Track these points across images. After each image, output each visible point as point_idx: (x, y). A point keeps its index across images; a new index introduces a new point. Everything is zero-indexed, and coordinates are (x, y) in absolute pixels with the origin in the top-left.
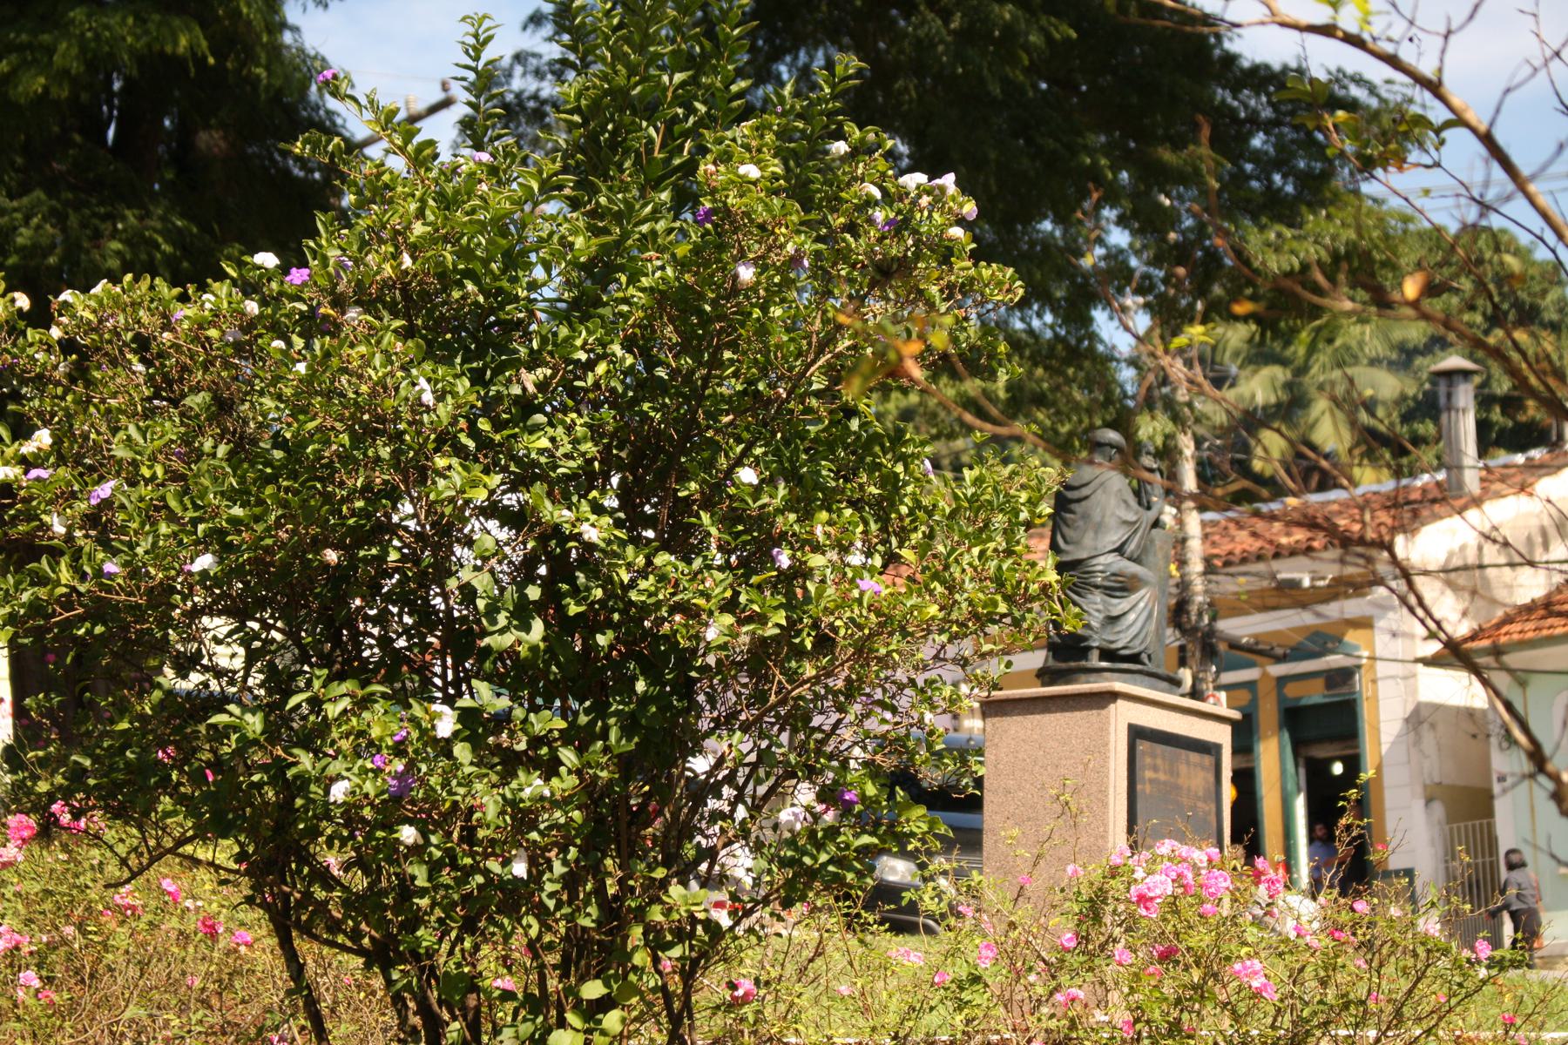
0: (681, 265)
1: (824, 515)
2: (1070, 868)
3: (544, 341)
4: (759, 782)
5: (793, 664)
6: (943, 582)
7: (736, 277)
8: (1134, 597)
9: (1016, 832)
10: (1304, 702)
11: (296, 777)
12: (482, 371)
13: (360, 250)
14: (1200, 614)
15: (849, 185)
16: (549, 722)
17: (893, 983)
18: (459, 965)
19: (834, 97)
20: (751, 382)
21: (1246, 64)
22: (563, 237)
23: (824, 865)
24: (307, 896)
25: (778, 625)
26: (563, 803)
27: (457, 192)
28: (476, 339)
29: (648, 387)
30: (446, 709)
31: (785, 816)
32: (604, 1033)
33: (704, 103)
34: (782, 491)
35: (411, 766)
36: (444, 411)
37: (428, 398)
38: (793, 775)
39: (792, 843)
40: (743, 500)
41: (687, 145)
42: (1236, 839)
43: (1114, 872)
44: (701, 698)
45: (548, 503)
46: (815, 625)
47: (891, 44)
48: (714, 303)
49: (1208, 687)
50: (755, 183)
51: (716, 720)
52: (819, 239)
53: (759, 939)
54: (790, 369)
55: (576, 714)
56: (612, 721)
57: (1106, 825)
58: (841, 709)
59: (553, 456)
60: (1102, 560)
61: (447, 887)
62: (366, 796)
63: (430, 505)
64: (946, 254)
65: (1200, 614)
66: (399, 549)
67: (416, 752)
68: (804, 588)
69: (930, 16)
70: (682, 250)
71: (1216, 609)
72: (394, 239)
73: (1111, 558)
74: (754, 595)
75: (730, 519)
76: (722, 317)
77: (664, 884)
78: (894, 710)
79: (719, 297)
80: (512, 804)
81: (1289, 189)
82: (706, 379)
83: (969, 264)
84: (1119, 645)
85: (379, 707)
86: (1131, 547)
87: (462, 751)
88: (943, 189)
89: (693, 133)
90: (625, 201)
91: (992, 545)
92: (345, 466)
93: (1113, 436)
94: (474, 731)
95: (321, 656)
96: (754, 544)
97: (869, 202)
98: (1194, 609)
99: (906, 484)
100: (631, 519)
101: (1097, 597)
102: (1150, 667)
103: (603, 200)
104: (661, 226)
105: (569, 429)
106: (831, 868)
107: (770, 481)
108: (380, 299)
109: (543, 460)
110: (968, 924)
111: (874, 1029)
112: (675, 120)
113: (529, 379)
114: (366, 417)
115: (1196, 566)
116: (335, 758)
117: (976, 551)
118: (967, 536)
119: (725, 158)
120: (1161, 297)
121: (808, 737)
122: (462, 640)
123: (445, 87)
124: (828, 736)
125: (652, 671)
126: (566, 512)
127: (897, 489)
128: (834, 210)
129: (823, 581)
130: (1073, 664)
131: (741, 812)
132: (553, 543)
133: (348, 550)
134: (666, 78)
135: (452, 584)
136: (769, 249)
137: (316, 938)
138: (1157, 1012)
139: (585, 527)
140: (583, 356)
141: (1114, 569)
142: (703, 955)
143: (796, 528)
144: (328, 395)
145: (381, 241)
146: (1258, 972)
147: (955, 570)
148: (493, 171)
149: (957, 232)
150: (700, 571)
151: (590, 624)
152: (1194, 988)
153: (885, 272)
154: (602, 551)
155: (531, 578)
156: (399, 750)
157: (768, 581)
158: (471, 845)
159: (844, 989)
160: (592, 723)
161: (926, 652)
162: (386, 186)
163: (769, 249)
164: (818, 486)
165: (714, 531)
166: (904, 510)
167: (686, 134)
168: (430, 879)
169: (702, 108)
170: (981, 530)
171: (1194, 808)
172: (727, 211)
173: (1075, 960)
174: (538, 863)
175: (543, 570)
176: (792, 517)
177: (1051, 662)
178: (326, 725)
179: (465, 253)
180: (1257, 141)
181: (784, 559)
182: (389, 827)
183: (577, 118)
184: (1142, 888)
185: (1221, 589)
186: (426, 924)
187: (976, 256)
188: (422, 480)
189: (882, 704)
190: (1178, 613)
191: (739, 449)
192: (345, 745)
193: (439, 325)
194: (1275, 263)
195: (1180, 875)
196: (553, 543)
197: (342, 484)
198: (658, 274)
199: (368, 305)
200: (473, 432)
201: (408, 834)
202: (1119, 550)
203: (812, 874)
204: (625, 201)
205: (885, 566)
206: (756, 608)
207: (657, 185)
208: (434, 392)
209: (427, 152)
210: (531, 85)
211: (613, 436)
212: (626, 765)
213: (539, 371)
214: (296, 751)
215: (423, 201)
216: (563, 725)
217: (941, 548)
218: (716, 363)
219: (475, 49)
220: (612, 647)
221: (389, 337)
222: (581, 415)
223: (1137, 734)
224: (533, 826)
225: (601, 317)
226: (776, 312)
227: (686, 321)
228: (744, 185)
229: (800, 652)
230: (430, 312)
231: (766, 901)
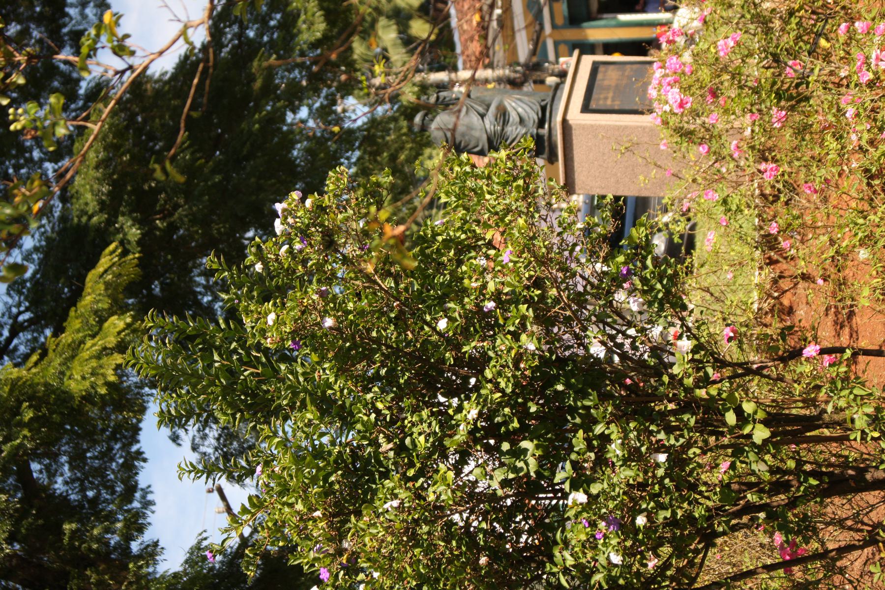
0: (323, 358)
1: (466, 281)
2: (662, 147)
3: (364, 438)
4: (615, 322)
5: (549, 301)
6: (506, 215)
7: (331, 328)
8: (509, 109)
9: (641, 178)
10: (566, 13)
11: (607, 583)
12: (380, 473)
13: (311, 540)
14: (516, 72)
15: (280, 263)
16: (579, 441)
17: (723, 249)
18: (715, 494)
19: (230, 270)
20: (390, 321)
21: (208, 39)
22: (305, 425)
23: (663, 286)
24: (672, 579)
25: (527, 310)
26: (625, 432)
27: (279, 484)
28: (363, 476)
29: (391, 380)
30: (571, 497)
31: (635, 308)
32: (755, 413)
33: (231, 343)
34: (451, 305)
35: (602, 517)
36: (403, 494)
37: (395, 503)
38: (611, 302)
39: (650, 304)
40: (457, 327)
41: (254, 354)
42: (644, 53)
43: (666, 123)
44: (567, 353)
45: (456, 437)
46: (527, 288)
47: (193, 239)
48: (345, 341)
49: (557, 68)
50: (278, 316)
51: (579, 345)
52: (310, 282)
53: (704, 323)
54: (382, 298)
55: (574, 424)
56: (579, 404)
57: (638, 127)
58: (574, 275)
59: (429, 435)
60: (488, 126)
61: (671, 499)
62: (619, 543)
63: (456, 504)
64: (321, 209)
65: (516, 72)
66: (480, 522)
67: (595, 514)
68: (506, 294)
69: (176, 215)
70: (315, 358)
71: (513, 63)
72: (305, 521)
73: (487, 121)
74: (510, 322)
75: (466, 333)
76: (353, 336)
77: (672, 377)
78: (575, 245)
79: (342, 338)
80: (626, 461)
81: (278, 16)
82: (388, 347)
83: (326, 197)
84: (536, 117)
85: (569, 535)
86: (481, 110)
87: (595, 489)
88: (284, 210)
89: (248, 351)
90: (286, 390)
91: (485, 188)
92: (432, 552)
93: (418, 119)
94: (584, 481)
95: (537, 569)
96: (481, 323)
97: (291, 251)
98: (513, 75)
99: (448, 234)
100: (460, 390)
101: (509, 129)
102: (549, 100)
103: (285, 402)
104: (300, 370)
105: (413, 425)
106: (665, 282)
107: (446, 311)
108: (338, 529)
109: (431, 440)
110: (693, 205)
111: (752, 260)
112: (240, 360)
113: (385, 446)
114: (405, 539)
115: (489, 73)
116: (596, 561)
117: (488, 197)
118: (479, 201)
119: (263, 332)
120: (338, 89)
121: (589, 294)
122: (527, 488)
123: (210, 491)
124: (589, 282)
125: (551, 381)
126: (461, 428)
127: (451, 240)
128: (294, 272)
129: (503, 283)
130: (546, 144)
131: (632, 332)
132: (478, 435)
133: (480, 550)
134: (217, 365)
135: (500, 492)
136: (316, 309)
137: (697, 575)
138: (747, 99)
139: (470, 417)
140: (373, 416)
141: (493, 119)
142: (712, 354)
143: (472, 297)
144: (392, 559)
145: (306, 528)
146: (725, 43)
147: (499, 208)
148: (267, 464)
149: (308, 203)
150: (496, 352)
151: (523, 413)
152: (733, 78)
153: (330, 244)
154: (483, 407)
155: (497, 448)
156: (593, 524)
157: (502, 315)
158: (648, 485)
159: (730, 276)
160: (580, 415)
161: (544, 226)
162: (275, 524)
163: (316, 309)
164: (449, 285)
165: (473, 344)
166: (463, 236)
167: (248, 354)
168: (667, 509)
169: (234, 345)
170: (476, 193)
171: (629, 78)
172: (294, 332)
173: (715, 146)
174: (660, 448)
175: (492, 442)
176: (466, 300)
177: (545, 156)
178: (578, 566)
179: (314, 480)
180: (251, 34)
181: (490, 305)
182: (637, 531)
183: (238, 416)
184: (675, 106)
185: (502, 59)
186: (691, 512)
187: (321, 194)
188: (441, 508)
189: (572, 251)
190: (515, 84)
191: (426, 328)
192: (589, 555)
193: (354, 498)
194: (321, 27)
195: (669, 84)
196: (478, 435)
197: (442, 554)
198: (328, 372)
199: (342, 536)
200: (415, 479)
201: (641, 521)
202: (482, 116)
203: (668, 293)
204: (286, 390)
205: (495, 248)
206: (517, 321)
207: (277, 371)
208: (392, 500)
209: (255, 500)
210: (211, 441)
211: (418, 401)
212: (604, 397)
213: (380, 441)
214: (592, 582)
215: (284, 504)
216: (581, 432)
217: (486, 216)
218: (378, 341)
219: (197, 473)
220: (537, 404)
221: (361, 524)
222: (406, 418)
223: (586, 108)
224: (638, 450)
225: (351, 405)
226: (350, 306)
227: (354, 357)
228: (279, 322)
229: (543, 298)
230: (346, 501)
231: (682, 319)
